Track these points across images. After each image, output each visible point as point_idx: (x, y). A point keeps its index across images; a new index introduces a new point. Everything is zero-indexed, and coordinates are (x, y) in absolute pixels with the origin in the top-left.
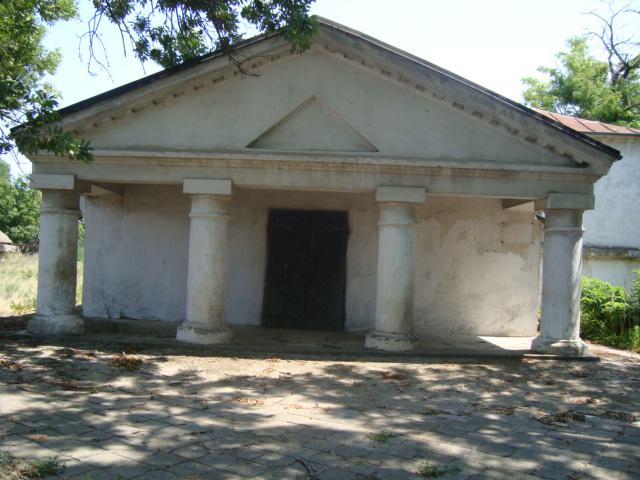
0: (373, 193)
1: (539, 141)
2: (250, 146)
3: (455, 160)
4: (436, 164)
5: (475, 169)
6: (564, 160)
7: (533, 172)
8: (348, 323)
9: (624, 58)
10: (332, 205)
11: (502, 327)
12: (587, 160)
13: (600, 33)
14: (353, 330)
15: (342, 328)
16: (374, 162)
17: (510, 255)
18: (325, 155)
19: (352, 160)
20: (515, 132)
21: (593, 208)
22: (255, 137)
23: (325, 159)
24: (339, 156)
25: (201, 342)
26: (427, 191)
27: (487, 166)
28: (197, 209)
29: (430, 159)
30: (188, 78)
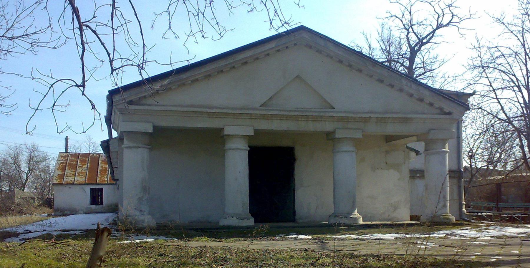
0: (223, 129)
1: (425, 100)
2: (262, 105)
3: (380, 113)
4: (368, 115)
5: (389, 118)
6: (438, 111)
7: (421, 118)
8: (297, 216)
9: (419, 36)
10: (285, 143)
11: (389, 216)
12: (451, 111)
13: (400, 16)
14: (301, 221)
15: (294, 220)
16: (335, 115)
17: (391, 171)
18: (307, 111)
19: (322, 114)
20: (411, 95)
21: (101, 142)
22: (265, 100)
23: (308, 114)
24: (315, 112)
25: (241, 225)
26: (362, 132)
27: (395, 116)
28: (230, 145)
29: (364, 113)
30: (228, 62)
